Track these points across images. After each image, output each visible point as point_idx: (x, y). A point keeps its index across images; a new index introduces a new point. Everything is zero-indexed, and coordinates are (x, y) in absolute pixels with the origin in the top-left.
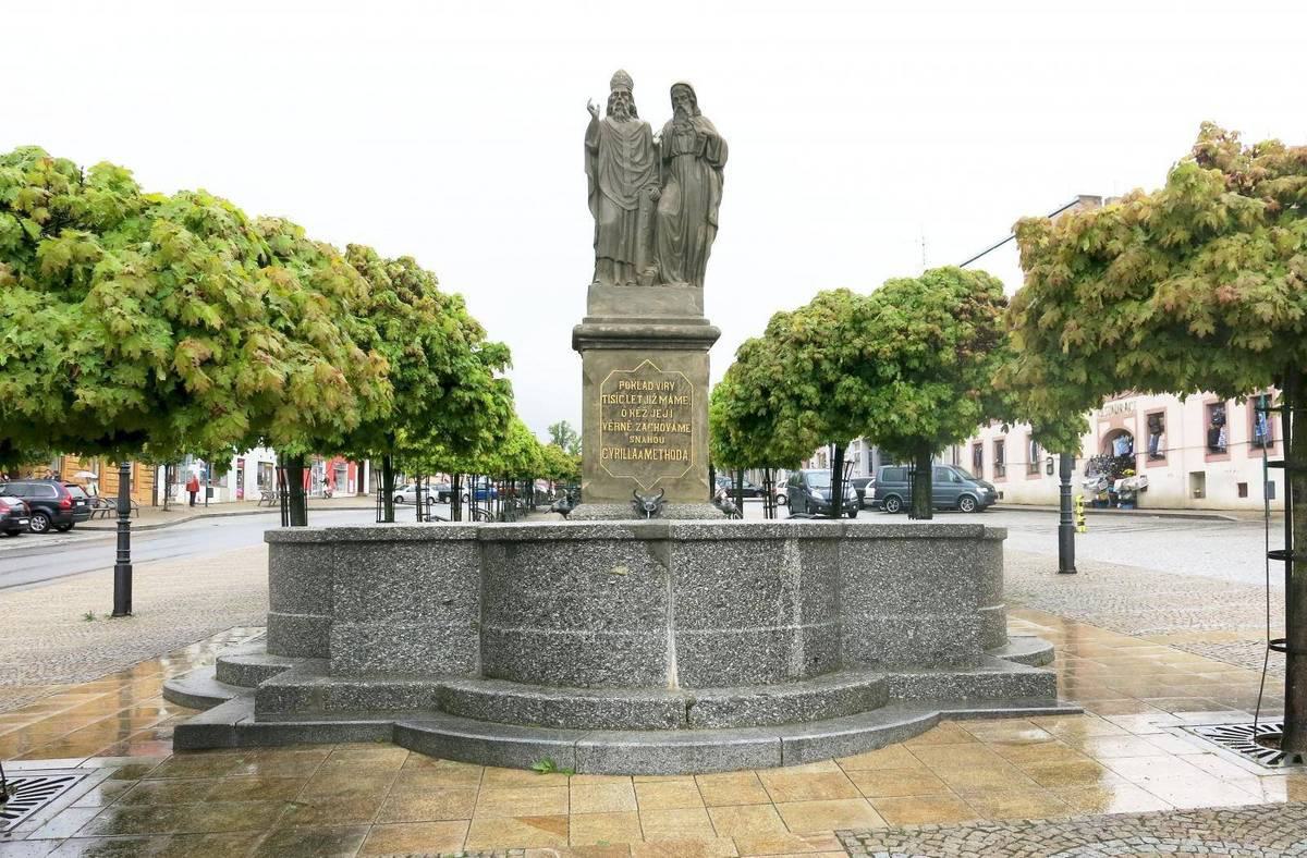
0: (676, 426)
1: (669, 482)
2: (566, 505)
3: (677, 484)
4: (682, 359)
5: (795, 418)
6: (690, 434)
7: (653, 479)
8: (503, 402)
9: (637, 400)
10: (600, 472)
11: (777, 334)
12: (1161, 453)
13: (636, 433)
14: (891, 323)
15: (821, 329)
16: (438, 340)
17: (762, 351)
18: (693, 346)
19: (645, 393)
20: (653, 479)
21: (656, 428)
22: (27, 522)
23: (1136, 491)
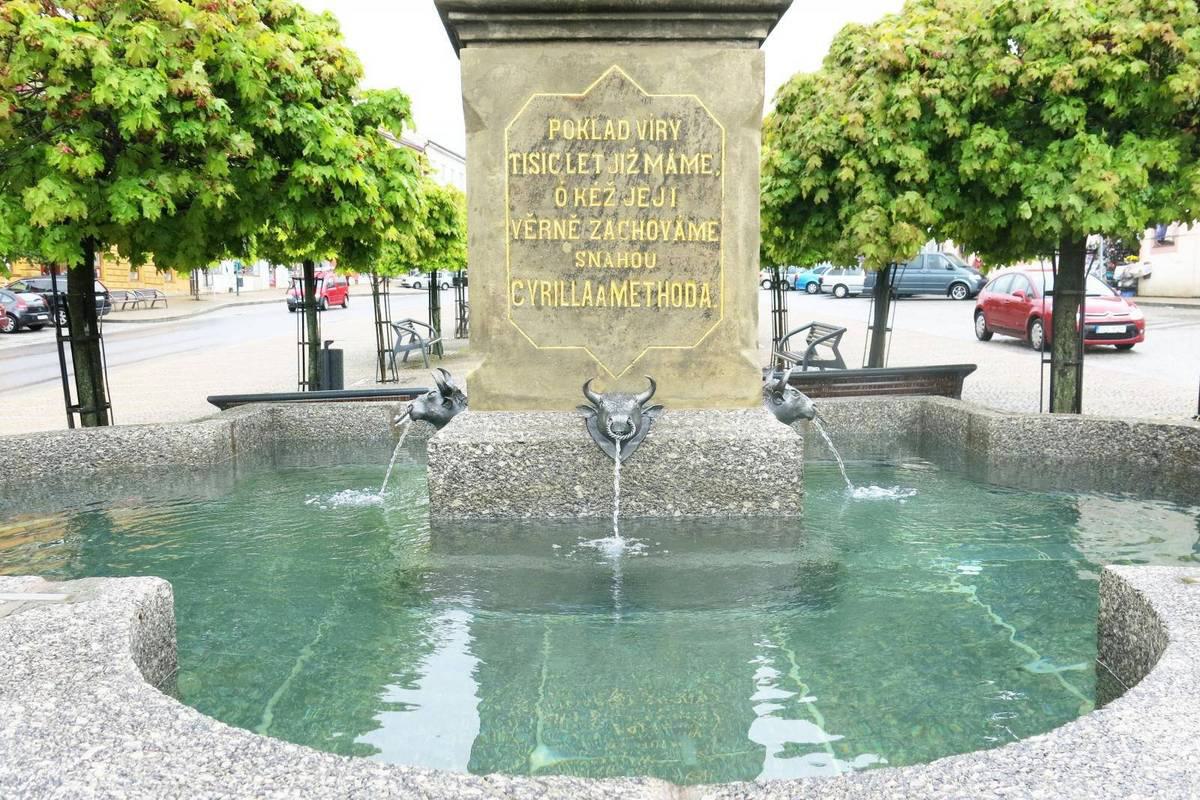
0: (685, 227)
1: (665, 360)
2: (438, 408)
3: (685, 364)
4: (697, 63)
5: (884, 204)
6: (716, 246)
7: (630, 352)
8: (401, 186)
9: (590, 164)
10: (507, 339)
11: (848, 61)
12: (1170, 239)
13: (590, 245)
14: (1073, 26)
15: (932, 45)
16: (247, 71)
17: (823, 90)
18: (728, 31)
19: (610, 147)
20: (630, 352)
21: (637, 232)
22: (45, 317)
23: (1137, 279)
